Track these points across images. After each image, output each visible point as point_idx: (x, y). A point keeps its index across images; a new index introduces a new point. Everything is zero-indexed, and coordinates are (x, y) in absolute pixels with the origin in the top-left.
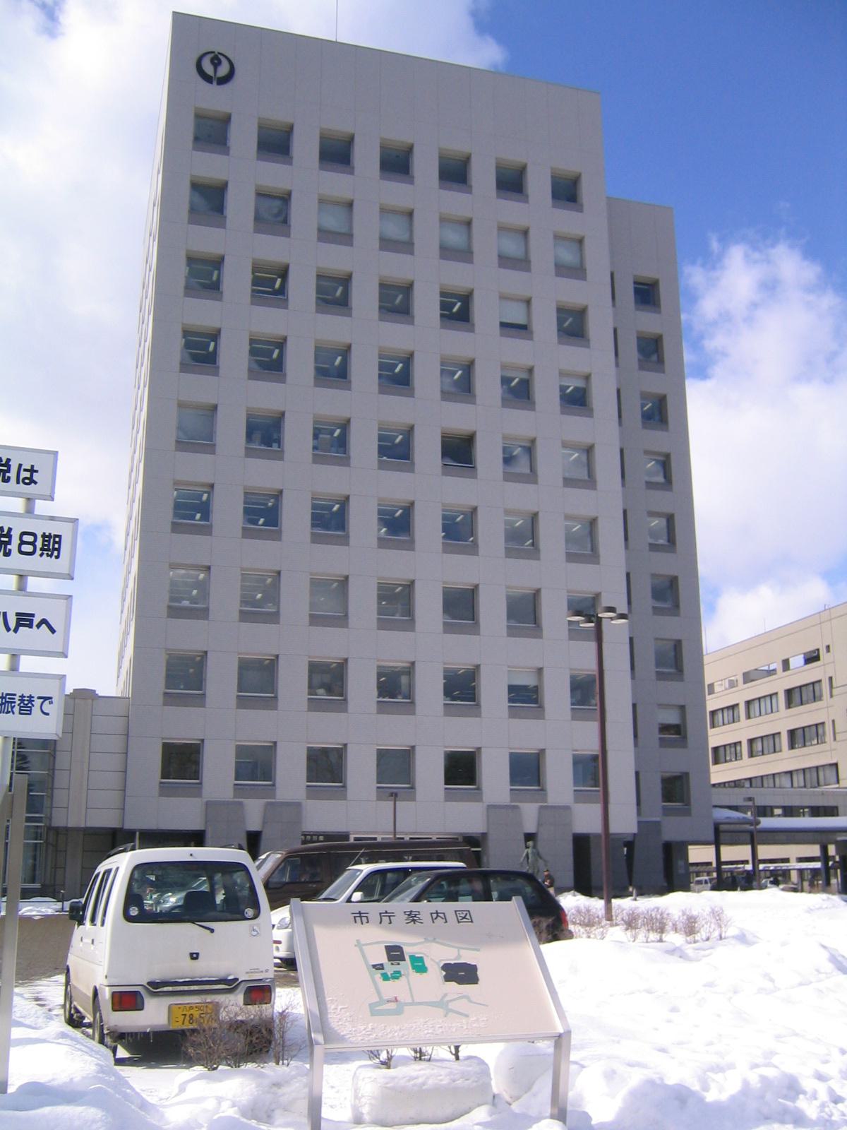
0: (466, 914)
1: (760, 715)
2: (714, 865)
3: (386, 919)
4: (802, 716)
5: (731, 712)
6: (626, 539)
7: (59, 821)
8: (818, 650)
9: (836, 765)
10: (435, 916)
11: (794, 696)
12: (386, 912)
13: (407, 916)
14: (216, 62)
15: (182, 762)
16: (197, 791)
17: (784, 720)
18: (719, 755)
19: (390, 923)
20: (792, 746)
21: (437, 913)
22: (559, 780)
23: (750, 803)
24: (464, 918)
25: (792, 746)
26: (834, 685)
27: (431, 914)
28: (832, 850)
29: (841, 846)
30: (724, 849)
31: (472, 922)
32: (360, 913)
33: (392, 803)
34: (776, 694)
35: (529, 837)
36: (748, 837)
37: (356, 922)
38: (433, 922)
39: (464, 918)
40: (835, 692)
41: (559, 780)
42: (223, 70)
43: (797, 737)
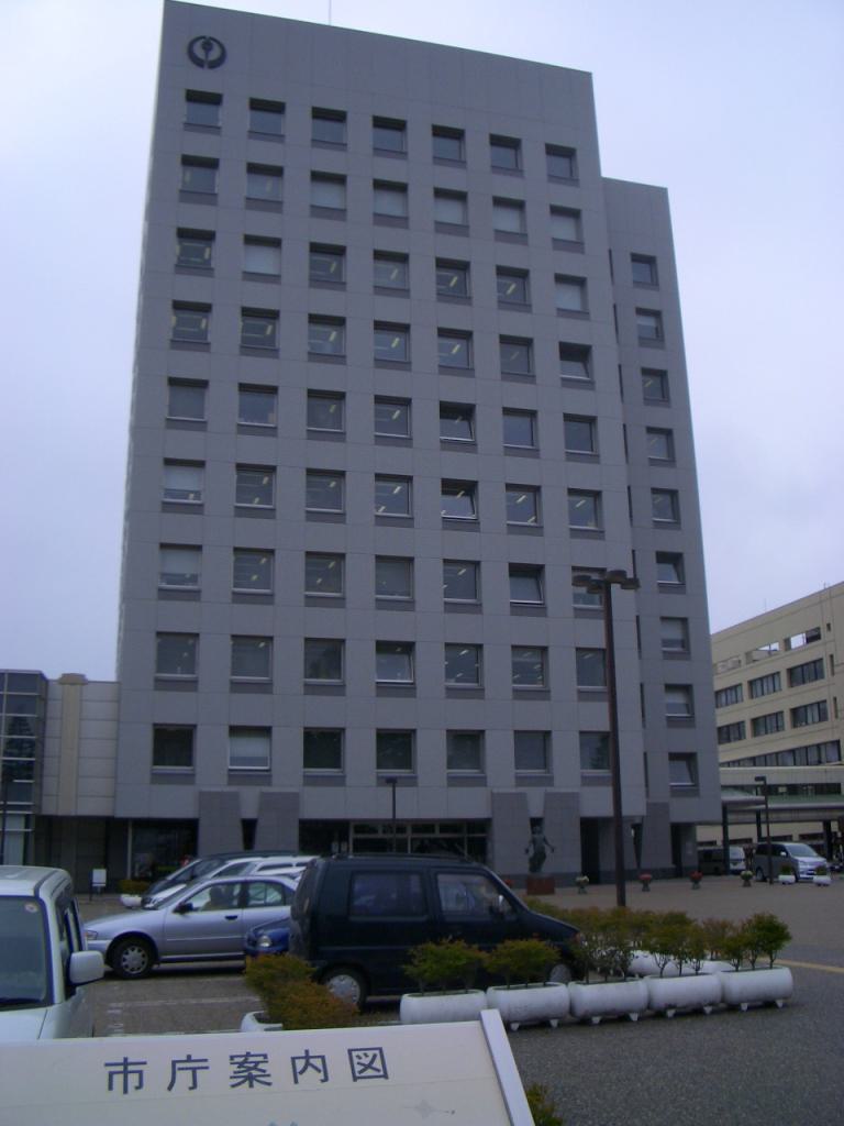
0: (375, 1056)
1: (763, 694)
2: (719, 843)
3: (184, 1078)
4: (807, 694)
5: (734, 693)
6: (631, 516)
7: (51, 808)
8: (819, 629)
9: (838, 742)
10: (300, 1064)
11: (798, 675)
12: (189, 1059)
13: (235, 1068)
14: (207, 46)
15: (174, 744)
16: (189, 779)
17: (786, 699)
18: (729, 733)
19: (194, 1086)
20: (756, 733)
21: (307, 1057)
22: (567, 758)
23: (762, 783)
24: (369, 1066)
25: (756, 733)
26: (835, 663)
27: (293, 1059)
28: (834, 826)
29: (840, 820)
30: (731, 829)
31: (385, 1076)
32: (126, 1063)
33: (391, 789)
34: (778, 673)
35: (536, 823)
36: (754, 817)
37: (110, 1087)
38: (296, 1081)
39: (369, 1066)
40: (836, 670)
41: (567, 758)
42: (215, 54)
43: (798, 715)
